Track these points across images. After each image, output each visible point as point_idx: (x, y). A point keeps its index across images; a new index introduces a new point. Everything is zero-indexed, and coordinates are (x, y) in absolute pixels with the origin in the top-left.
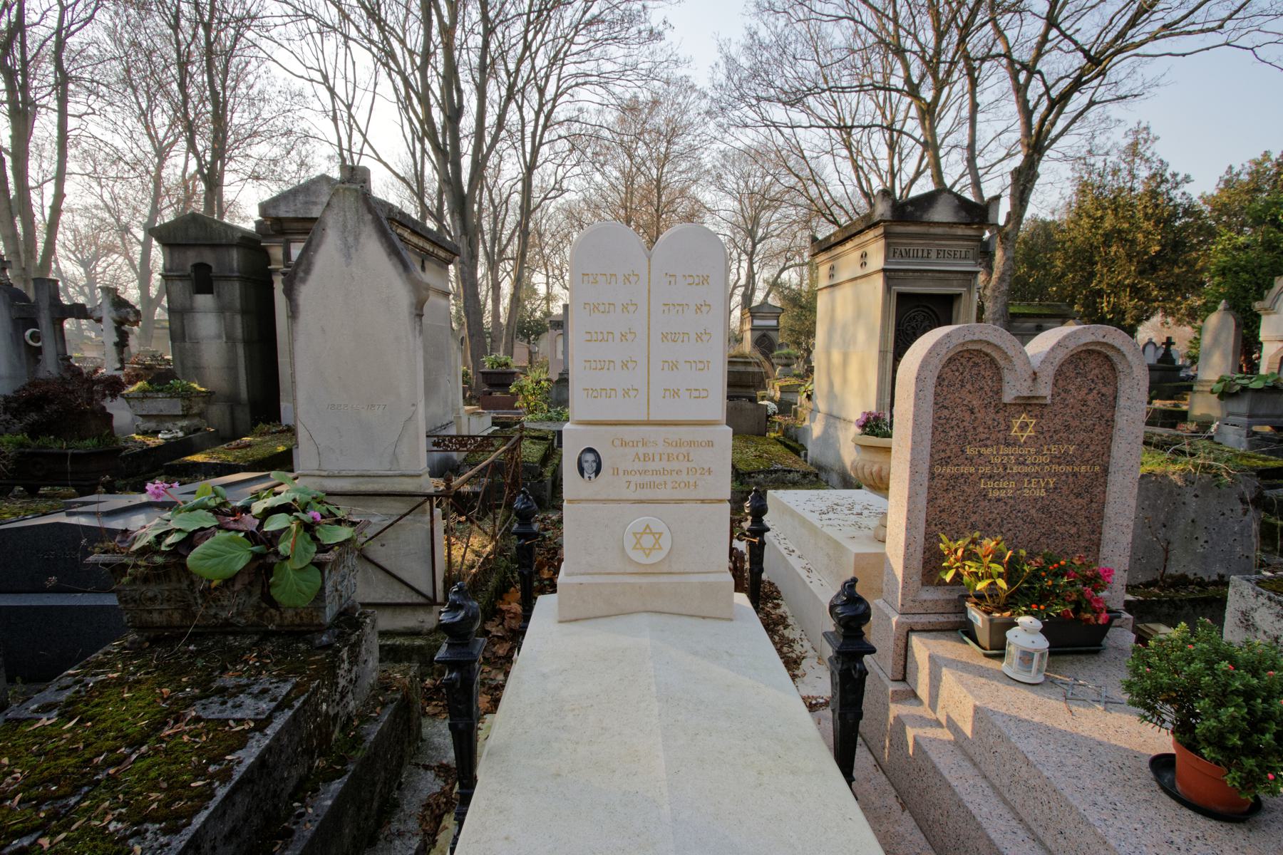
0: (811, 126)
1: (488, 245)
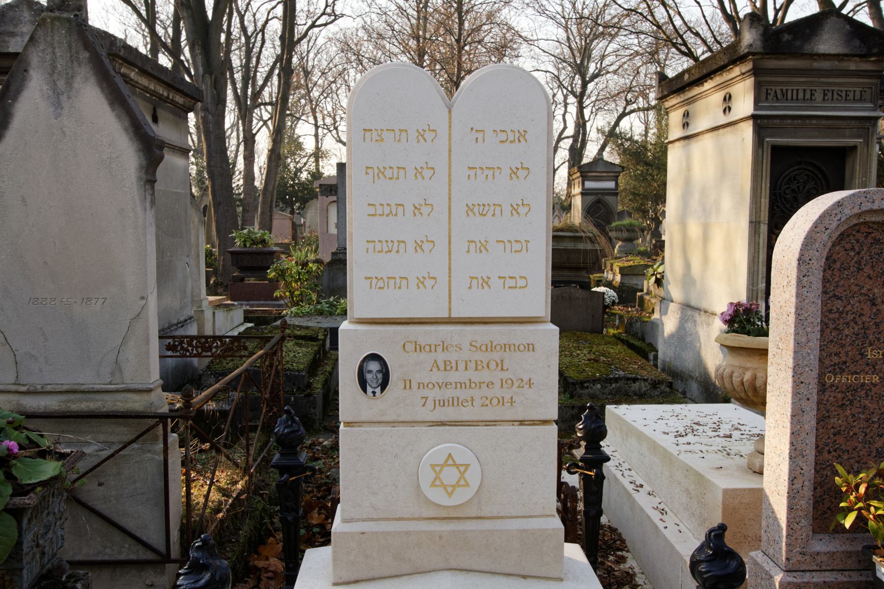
1: (239, 85)
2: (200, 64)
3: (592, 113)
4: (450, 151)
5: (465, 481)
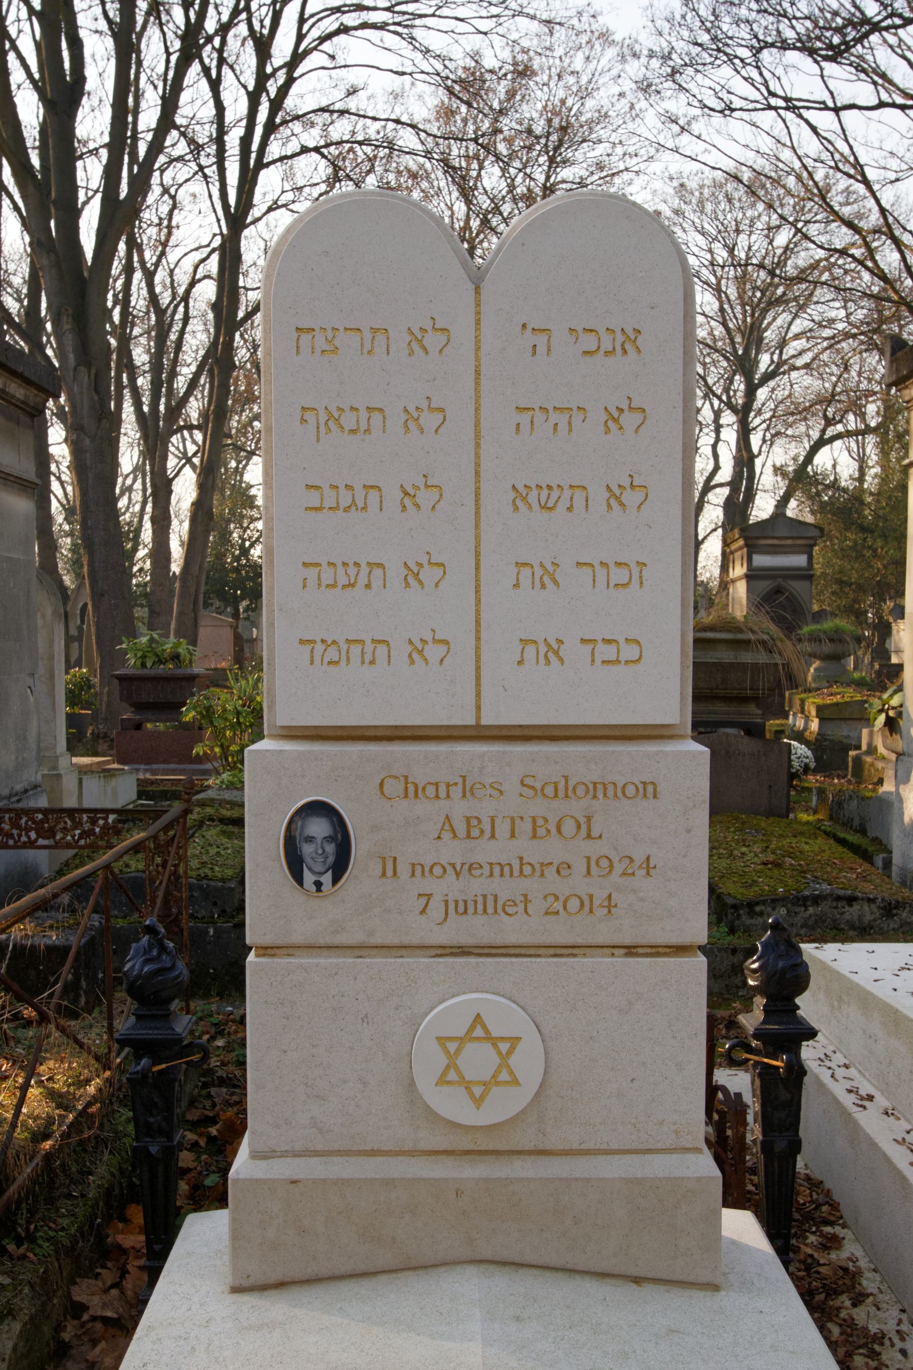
0: (881, 105)
1: (146, 400)
2: (69, 349)
3: (764, 441)
4: (478, 373)
5: (511, 1073)
